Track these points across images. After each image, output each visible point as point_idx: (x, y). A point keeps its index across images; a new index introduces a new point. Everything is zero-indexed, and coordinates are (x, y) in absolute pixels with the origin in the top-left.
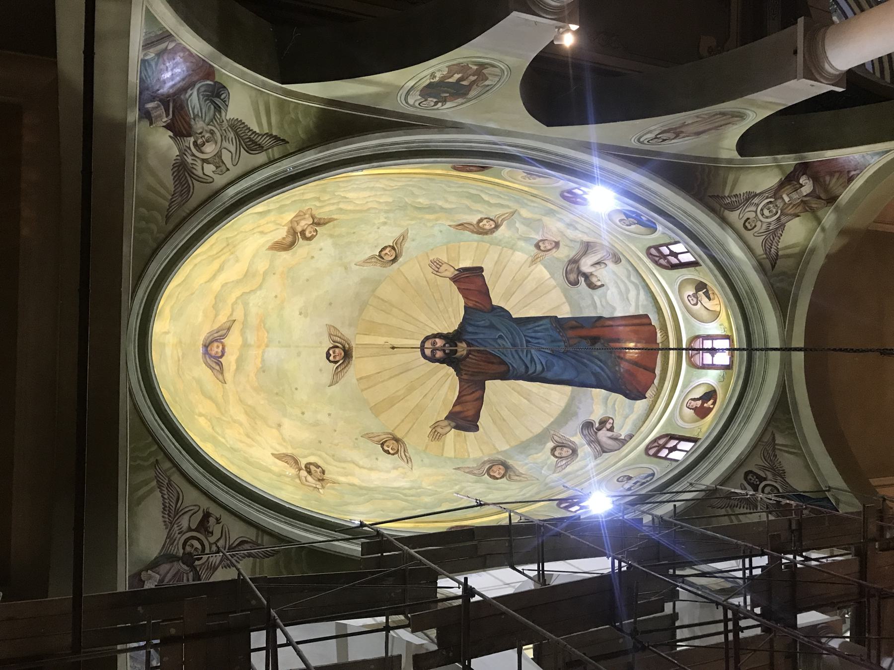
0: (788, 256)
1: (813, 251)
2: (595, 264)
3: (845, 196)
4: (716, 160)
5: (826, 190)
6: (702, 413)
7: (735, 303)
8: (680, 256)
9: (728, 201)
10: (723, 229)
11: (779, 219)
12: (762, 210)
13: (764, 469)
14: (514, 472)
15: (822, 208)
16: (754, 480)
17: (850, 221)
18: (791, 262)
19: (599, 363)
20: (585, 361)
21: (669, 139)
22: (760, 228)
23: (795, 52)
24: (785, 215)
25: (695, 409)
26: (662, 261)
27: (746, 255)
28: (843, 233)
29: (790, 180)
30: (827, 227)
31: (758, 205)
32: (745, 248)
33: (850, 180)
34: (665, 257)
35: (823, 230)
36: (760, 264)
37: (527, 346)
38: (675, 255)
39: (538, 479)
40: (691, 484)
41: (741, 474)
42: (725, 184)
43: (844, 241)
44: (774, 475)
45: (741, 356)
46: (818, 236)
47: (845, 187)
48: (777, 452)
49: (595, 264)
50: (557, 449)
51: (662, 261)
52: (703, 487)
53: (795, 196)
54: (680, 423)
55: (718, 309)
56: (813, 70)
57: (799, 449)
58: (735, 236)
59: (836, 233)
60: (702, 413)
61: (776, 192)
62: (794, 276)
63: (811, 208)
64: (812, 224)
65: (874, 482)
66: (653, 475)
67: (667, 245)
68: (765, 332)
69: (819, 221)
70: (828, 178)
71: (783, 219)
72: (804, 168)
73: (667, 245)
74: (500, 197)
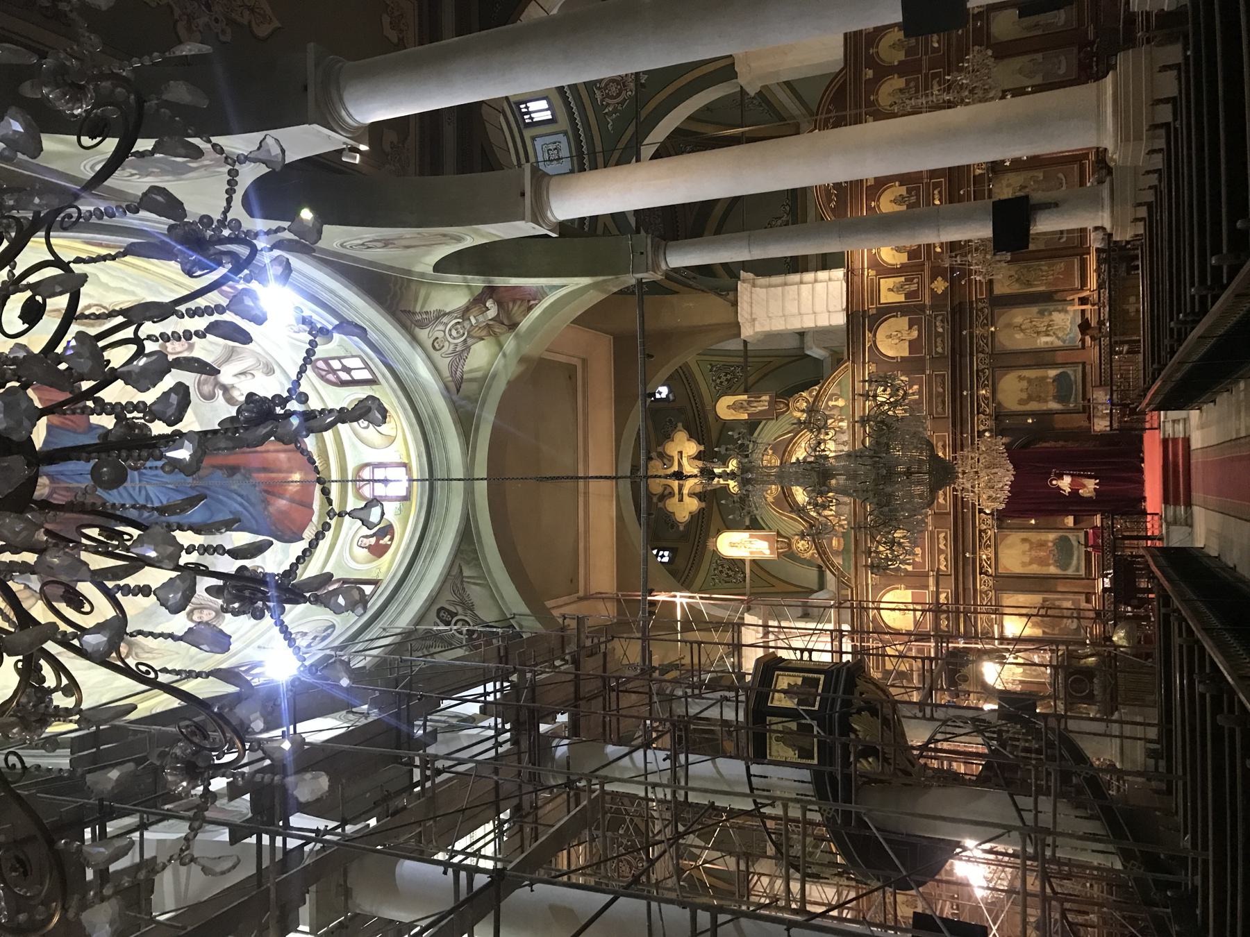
0: (471, 380)
1: (494, 376)
2: (241, 374)
3: (525, 323)
4: (409, 272)
5: (509, 316)
6: (378, 551)
7: (417, 428)
8: (353, 373)
9: (419, 317)
10: (413, 347)
11: (465, 341)
12: (450, 330)
13: (454, 603)
14: (143, 649)
15: (504, 333)
16: (445, 616)
17: (527, 349)
18: (474, 386)
19: (239, 499)
20: (221, 497)
21: (376, 247)
22: (448, 348)
23: (523, 194)
24: (473, 336)
25: (369, 548)
26: (331, 377)
27: (433, 375)
28: (523, 360)
29: (478, 301)
30: (508, 352)
31: (446, 324)
32: (431, 367)
33: (530, 308)
34: (334, 371)
35: (504, 355)
36: (447, 388)
37: (140, 481)
38: (347, 370)
39: (177, 653)
40: (384, 629)
41: (433, 613)
42: (416, 300)
43: (521, 368)
44: (464, 609)
45: (423, 487)
46: (499, 362)
47: (525, 316)
48: (465, 584)
49: (241, 374)
50: (195, 612)
51: (331, 377)
52: (399, 631)
53: (481, 318)
54: (353, 565)
55: (393, 434)
56: (538, 215)
57: (484, 579)
58: (424, 356)
59: (515, 361)
60: (378, 551)
61: (465, 312)
62: (477, 401)
63: (494, 332)
64: (495, 349)
65: (549, 604)
66: (333, 626)
67: (339, 358)
68: (447, 459)
69: (501, 346)
70: (511, 305)
71: (470, 341)
72: (491, 291)
73: (339, 358)
74: (126, 281)
